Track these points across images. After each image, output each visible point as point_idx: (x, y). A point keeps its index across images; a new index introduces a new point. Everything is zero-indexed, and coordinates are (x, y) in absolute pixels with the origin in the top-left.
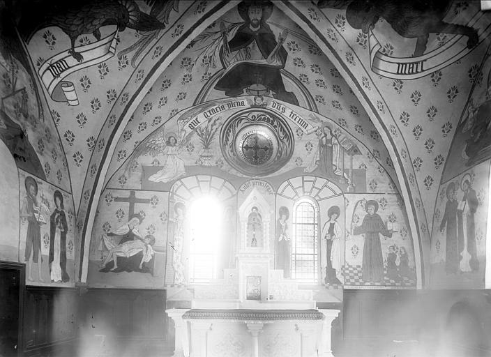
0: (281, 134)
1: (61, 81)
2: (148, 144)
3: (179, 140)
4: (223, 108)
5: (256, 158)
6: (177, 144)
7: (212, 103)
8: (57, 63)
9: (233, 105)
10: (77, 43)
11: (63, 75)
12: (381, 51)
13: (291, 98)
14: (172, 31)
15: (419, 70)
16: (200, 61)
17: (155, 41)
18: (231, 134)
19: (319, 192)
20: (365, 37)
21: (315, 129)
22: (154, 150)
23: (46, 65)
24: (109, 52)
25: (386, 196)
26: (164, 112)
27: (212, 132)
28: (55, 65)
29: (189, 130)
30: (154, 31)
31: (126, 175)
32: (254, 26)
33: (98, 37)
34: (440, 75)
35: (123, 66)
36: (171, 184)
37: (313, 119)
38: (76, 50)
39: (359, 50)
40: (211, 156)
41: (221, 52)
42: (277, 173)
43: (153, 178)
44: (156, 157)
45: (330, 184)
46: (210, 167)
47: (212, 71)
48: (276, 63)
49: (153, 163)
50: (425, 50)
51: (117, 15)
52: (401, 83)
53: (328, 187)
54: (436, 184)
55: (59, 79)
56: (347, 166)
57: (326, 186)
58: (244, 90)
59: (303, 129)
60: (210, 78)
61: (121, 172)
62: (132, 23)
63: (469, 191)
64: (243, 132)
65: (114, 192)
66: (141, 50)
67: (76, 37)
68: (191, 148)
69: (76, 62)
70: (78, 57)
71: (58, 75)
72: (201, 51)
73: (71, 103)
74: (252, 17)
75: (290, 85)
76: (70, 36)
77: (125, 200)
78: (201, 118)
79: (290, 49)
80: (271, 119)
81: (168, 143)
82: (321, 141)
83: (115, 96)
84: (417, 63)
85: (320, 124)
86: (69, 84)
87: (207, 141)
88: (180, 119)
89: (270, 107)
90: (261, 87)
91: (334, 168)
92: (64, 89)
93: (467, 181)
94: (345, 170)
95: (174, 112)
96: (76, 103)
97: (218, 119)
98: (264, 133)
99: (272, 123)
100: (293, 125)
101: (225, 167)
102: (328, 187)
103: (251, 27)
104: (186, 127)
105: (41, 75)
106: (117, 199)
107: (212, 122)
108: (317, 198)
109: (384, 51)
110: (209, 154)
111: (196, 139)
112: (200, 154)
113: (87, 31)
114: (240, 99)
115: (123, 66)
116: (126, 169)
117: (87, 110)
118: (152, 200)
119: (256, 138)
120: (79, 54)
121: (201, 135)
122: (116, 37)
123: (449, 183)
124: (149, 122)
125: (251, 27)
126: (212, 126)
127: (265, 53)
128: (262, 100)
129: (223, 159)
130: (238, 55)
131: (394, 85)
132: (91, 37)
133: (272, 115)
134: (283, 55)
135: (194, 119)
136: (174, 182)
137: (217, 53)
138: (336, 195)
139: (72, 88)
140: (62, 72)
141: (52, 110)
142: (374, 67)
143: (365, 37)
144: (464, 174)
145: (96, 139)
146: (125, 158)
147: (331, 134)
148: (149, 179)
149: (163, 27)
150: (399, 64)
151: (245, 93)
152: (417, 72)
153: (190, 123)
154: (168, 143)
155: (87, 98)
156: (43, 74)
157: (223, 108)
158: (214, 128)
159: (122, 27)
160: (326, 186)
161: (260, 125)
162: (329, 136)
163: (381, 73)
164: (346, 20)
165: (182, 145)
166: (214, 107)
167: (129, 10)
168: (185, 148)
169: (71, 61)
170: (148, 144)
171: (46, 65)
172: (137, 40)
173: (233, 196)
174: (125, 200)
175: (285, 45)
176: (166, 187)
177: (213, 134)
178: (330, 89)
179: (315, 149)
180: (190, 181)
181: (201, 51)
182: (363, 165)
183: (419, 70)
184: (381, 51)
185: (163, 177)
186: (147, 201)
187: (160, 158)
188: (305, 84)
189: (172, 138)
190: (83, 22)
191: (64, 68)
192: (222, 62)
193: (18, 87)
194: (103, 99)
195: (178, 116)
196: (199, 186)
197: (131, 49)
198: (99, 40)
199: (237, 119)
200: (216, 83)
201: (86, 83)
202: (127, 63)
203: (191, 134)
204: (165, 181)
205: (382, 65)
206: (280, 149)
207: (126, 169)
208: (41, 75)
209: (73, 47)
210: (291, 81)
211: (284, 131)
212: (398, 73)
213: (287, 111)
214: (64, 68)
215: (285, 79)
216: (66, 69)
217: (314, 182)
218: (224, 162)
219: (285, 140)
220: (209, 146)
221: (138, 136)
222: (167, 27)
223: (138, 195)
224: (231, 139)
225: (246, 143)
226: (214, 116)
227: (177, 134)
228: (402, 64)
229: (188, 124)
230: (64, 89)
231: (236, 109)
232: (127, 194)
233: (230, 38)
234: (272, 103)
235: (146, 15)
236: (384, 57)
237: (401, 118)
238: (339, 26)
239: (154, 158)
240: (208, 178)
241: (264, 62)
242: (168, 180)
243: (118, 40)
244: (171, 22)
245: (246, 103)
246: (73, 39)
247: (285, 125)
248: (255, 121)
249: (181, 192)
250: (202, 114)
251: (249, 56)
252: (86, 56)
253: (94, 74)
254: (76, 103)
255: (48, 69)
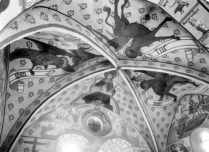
0: (105, 121)
1: (19, 81)
2: (47, 117)
3: (62, 117)
4: (83, 107)
5: (94, 129)
6: (61, 119)
7: (78, 104)
8: (21, 73)
9: (87, 106)
10: (35, 67)
11: (20, 78)
12: (149, 97)
13: (111, 108)
14: (78, 74)
15: (160, 105)
16: (82, 87)
17: (69, 75)
18: (85, 118)
19: (122, 146)
20: (145, 92)
21: (119, 120)
22: (50, 120)
23: (15, 72)
24: (48, 75)
25: (147, 149)
26: (57, 104)
27: (78, 116)
28: (20, 73)
29: (68, 114)
30: (70, 72)
31: (33, 130)
32: (108, 80)
33: (46, 67)
34: (166, 108)
35: (205, 61)
36: (58, 136)
37: (118, 117)
38: (33, 70)
39: (142, 95)
40: (78, 126)
41: (91, 86)
42: (106, 136)
43: (48, 133)
44: (50, 123)
45: (127, 142)
46: (77, 130)
47: (84, 92)
48: (109, 93)
49: (49, 126)
50: (162, 99)
51: (58, 63)
52: (154, 108)
53: (126, 144)
54: (165, 144)
55: (18, 80)
56: (132, 136)
57: (125, 143)
58: (93, 102)
59: (115, 120)
60: (82, 95)
61: (30, 128)
62: (63, 67)
63: (182, 147)
64: (89, 118)
65: (24, 138)
66: (61, 78)
67: (36, 65)
68: (68, 121)
69: (30, 74)
70: (33, 73)
71: (19, 78)
72: (84, 84)
73: (19, 91)
74: (108, 77)
75: (112, 103)
76: (33, 64)
77: (31, 143)
78: (73, 109)
79: (117, 90)
80: (102, 114)
81: (57, 117)
82: (122, 125)
83: (42, 93)
84: (160, 103)
85: (120, 119)
86: (22, 83)
87: (76, 119)
88: (63, 108)
89: (102, 110)
90: (100, 102)
91: (128, 136)
92: (18, 84)
93: (180, 144)
94: (132, 137)
95: (62, 105)
96: (22, 91)
97: (81, 111)
98: (96, 119)
99: (102, 116)
100: (111, 118)
101: (84, 131)
102: (126, 144)
103: (106, 80)
104: (66, 112)
105: (10, 76)
106: (26, 142)
107: (78, 112)
108: (121, 148)
109: (150, 97)
110: (77, 125)
111: (70, 117)
112: (73, 124)
113: (43, 65)
114: (90, 105)
115: (205, 61)
116: (33, 127)
117: (25, 95)
118: (47, 143)
119: (94, 122)
120: (34, 72)
121: (73, 116)
122: (54, 70)
123: (171, 144)
124: (50, 107)
125: (106, 80)
126: (78, 113)
127: (107, 90)
128: (99, 107)
129: (83, 127)
130: (97, 89)
131: (152, 109)
132: (43, 67)
133: (102, 113)
134: (114, 92)
135: (70, 109)
136: (59, 136)
137: (90, 86)
138: (129, 147)
139: (23, 85)
140: (21, 77)
141: (7, 92)
142: (146, 102)
143: (145, 92)
144: (178, 141)
145: (24, 110)
146: (34, 122)
147: (125, 123)
148: (46, 133)
149: (75, 71)
150: (154, 102)
151: (93, 103)
152: (159, 106)
153: (68, 110)
154: (57, 117)
155: (27, 91)
156: (10, 76)
157: (83, 107)
158: (79, 114)
159: (58, 67)
160: (125, 143)
161: (96, 116)
162: (124, 124)
163: (148, 104)
164: (140, 86)
165: (64, 119)
166: (79, 106)
167: (64, 61)
168: (65, 121)
169: (29, 74)
170: (47, 117)
171: (15, 72)
172: (62, 73)
173: (87, 144)
174: (31, 143)
175: (116, 89)
176: (54, 138)
177: (79, 116)
178: (127, 107)
179: (120, 128)
180: (67, 136)
181: (84, 84)
182: (137, 136)
183: (160, 105)
184: (149, 97)
185: (54, 133)
186: (44, 144)
187: (53, 124)
188: (118, 103)
189: (59, 116)
190: (42, 61)
191: (23, 76)
192: (90, 90)
193: (3, 78)
194: (36, 93)
195: (63, 107)
196: (70, 139)
197: (58, 76)
198: (46, 69)
199: (88, 112)
200: (84, 97)
201: (31, 84)
202: (53, 81)
203: (68, 115)
204: (54, 135)
205: (149, 102)
206: (105, 126)
207: (33, 127)
208: (10, 76)
209: (32, 69)
210: (113, 102)
211: (107, 120)
212: (153, 105)
213: (108, 112)
214: (23, 76)
215: (111, 101)
216: (24, 76)
217: (121, 141)
218: (84, 129)
219: (107, 123)
220: (77, 121)
221: (43, 113)
222: (76, 72)
223: (39, 140)
224: (85, 120)
225: (90, 123)
226: (79, 110)
227: (62, 114)
228: (155, 102)
229: (67, 111)
230: (18, 84)
231: (88, 108)
232: (32, 140)
233: (97, 82)
234: (102, 108)
235: (70, 66)
236: (149, 99)
237: (153, 120)
238: (137, 87)
239: (50, 124)
240: (76, 135)
241: (106, 93)
242: (56, 134)
243: (54, 71)
244: (79, 71)
245: (92, 107)
246: (34, 66)
247: (107, 117)
248: (95, 114)
249: (61, 139)
250: (73, 108)
251: (101, 89)
252: (36, 74)
253: (36, 82)
254: (22, 91)
255: (15, 74)
